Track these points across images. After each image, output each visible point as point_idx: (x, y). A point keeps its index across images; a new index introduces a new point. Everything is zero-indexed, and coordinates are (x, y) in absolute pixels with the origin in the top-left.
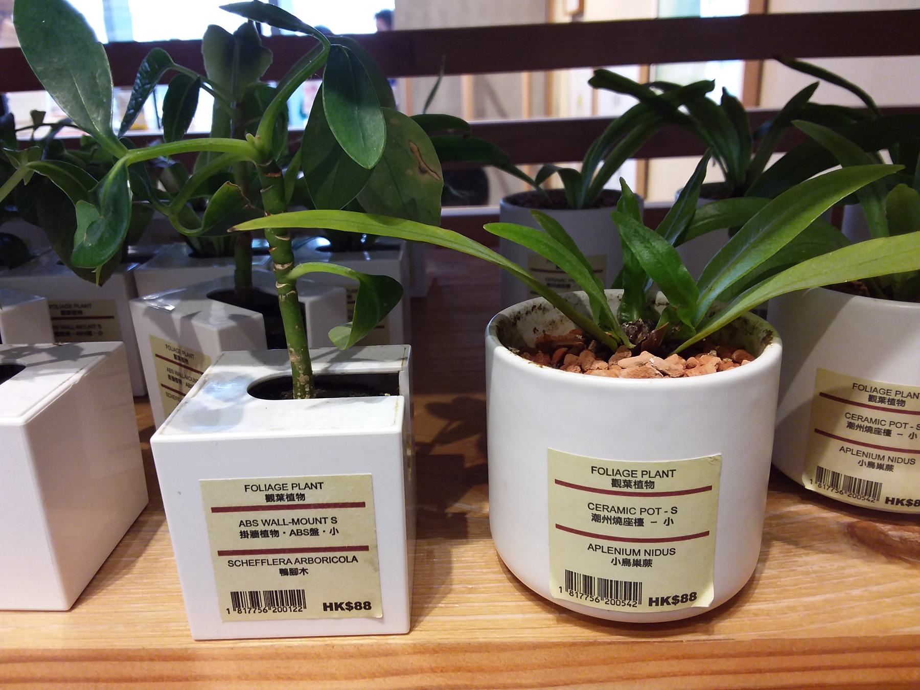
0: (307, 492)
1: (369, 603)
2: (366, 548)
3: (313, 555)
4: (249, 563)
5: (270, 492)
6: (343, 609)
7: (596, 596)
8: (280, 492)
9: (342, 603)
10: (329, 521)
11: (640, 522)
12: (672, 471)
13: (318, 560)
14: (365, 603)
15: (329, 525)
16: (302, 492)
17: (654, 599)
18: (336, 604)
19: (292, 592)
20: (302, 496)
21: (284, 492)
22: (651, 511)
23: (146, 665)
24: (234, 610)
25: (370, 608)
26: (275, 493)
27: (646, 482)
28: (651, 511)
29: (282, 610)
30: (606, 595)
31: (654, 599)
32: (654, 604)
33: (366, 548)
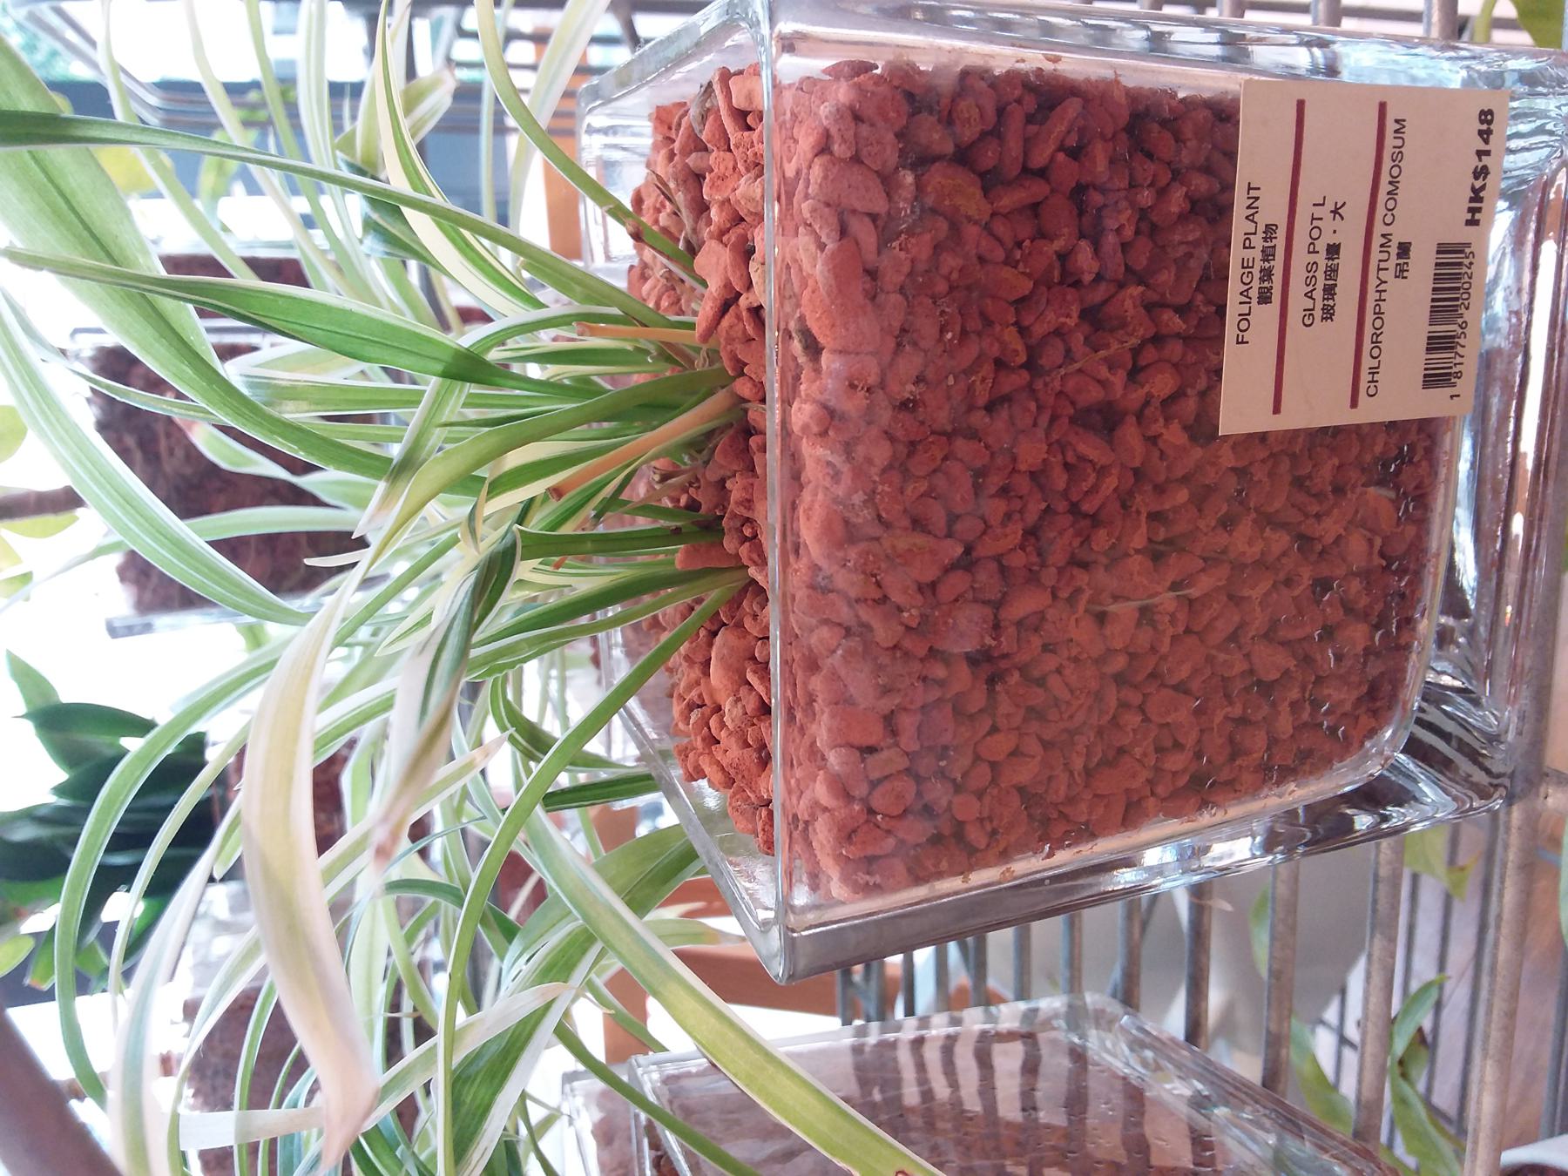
0: (1262, 219)
1: (1482, 112)
2: (1382, 107)
3: (1385, 178)
4: (1374, 371)
5: (1254, 293)
6: (1483, 188)
7: (1455, 327)
8: (1257, 275)
9: (1473, 189)
10: (1318, 212)
11: (1333, 250)
12: (1250, 189)
13: (1378, 323)
14: (1482, 122)
15: (1328, 224)
16: (1261, 228)
17: (1469, 216)
18: (1472, 200)
19: (1437, 278)
20: (1270, 229)
21: (1258, 265)
22: (1315, 233)
23: (1499, 1006)
24: (1454, 385)
25: (1490, 112)
26: (1256, 284)
27: (1265, 240)
28: (1315, 233)
29: (1467, 291)
30: (1455, 309)
31: (1469, 216)
32: (1477, 216)
33: (1382, 107)
